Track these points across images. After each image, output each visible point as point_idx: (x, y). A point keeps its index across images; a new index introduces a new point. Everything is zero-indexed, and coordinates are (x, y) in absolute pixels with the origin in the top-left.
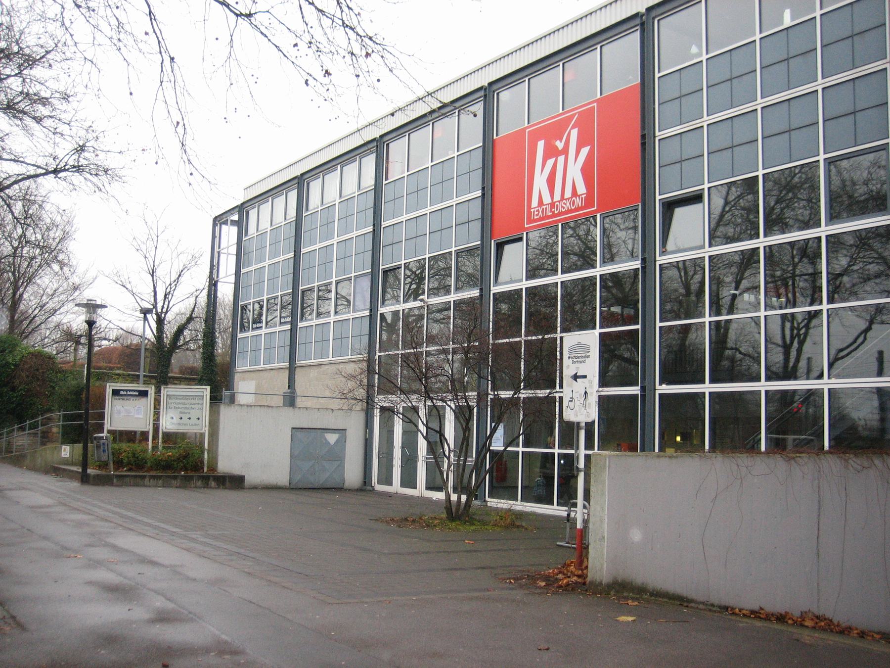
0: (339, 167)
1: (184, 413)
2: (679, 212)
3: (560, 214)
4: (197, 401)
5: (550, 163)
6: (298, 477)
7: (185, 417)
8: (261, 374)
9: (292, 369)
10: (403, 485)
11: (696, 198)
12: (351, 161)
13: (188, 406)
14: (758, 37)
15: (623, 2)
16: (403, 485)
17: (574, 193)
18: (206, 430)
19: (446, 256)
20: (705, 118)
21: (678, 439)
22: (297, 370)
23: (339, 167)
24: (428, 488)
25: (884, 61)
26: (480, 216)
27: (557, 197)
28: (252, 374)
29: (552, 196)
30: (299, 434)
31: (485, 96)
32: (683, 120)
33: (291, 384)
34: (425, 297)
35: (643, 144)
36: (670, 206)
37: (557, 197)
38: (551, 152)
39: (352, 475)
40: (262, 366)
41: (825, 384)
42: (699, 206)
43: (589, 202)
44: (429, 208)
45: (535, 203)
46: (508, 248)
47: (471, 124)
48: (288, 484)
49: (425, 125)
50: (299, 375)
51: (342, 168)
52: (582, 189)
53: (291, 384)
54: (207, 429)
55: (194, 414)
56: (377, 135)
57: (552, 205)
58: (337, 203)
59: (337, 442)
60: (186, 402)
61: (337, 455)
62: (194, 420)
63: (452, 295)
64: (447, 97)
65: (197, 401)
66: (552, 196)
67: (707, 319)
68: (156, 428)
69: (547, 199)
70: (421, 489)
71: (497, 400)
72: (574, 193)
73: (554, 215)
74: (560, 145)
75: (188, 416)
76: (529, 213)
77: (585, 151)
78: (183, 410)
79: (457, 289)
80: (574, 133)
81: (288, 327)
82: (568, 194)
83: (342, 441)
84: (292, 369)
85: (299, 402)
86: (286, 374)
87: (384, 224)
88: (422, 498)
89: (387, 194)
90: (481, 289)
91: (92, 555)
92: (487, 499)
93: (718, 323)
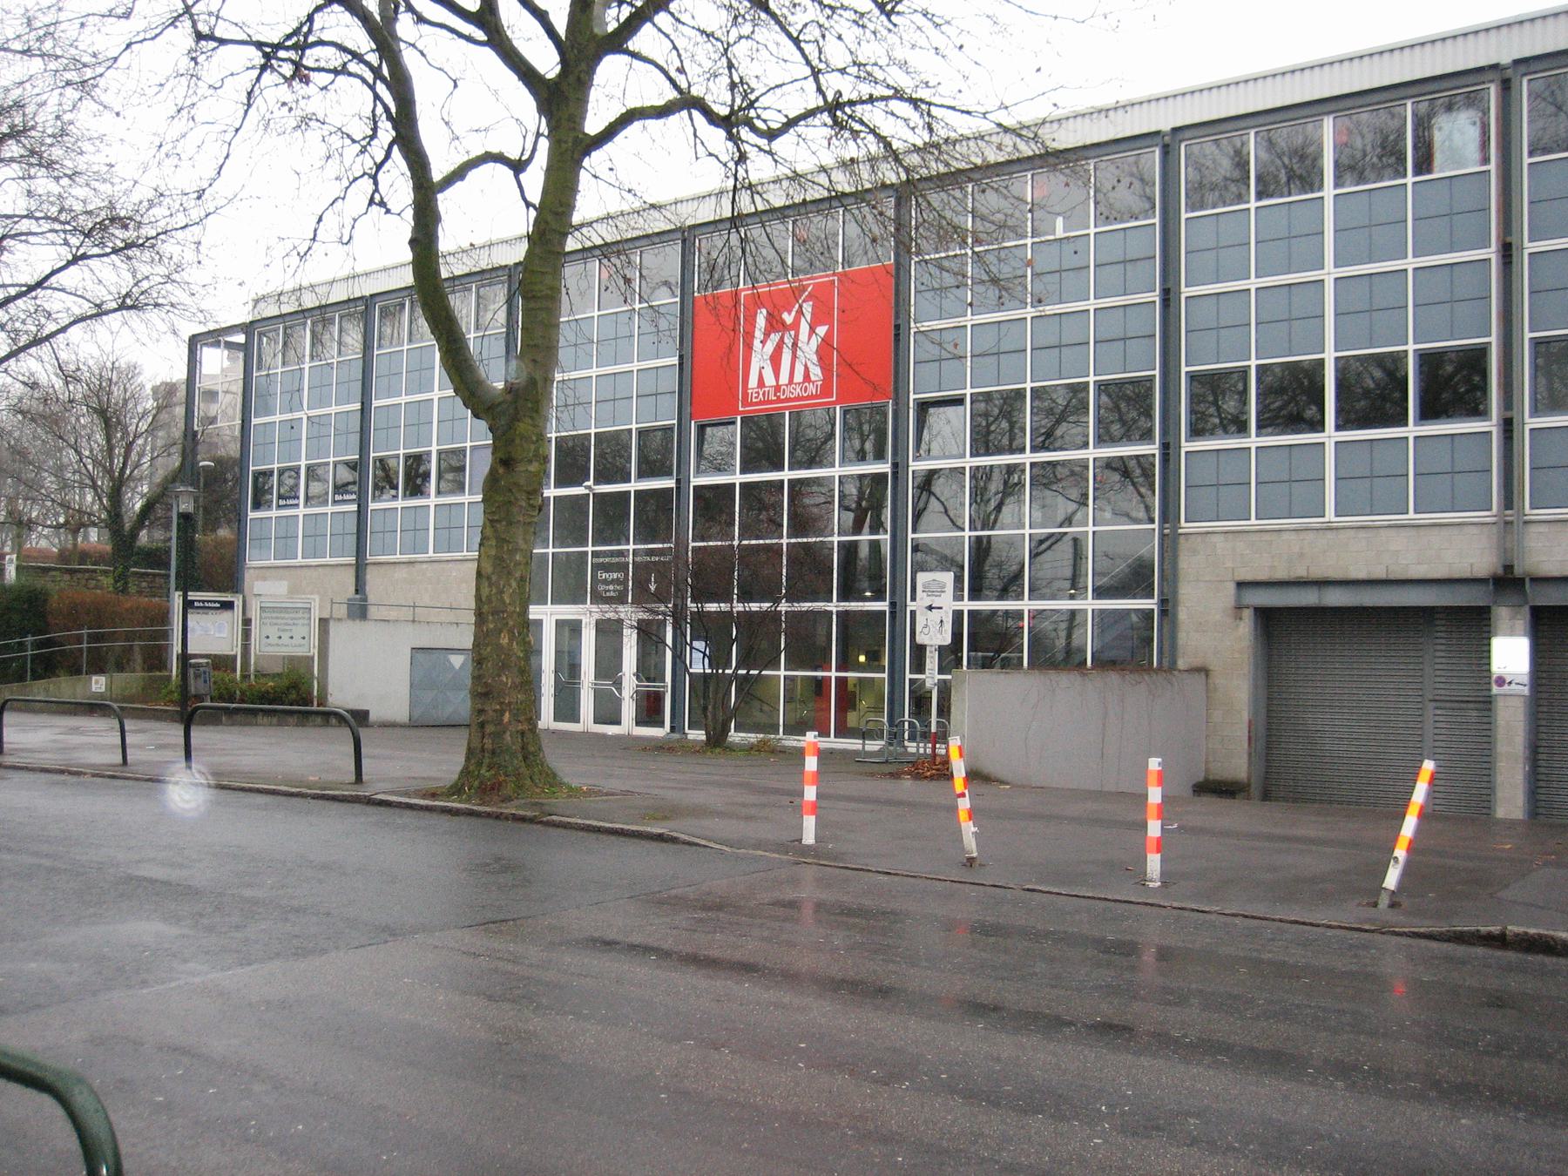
3: (788, 400)
5: (775, 337)
6: (416, 715)
7: (285, 636)
8: (299, 571)
9: (360, 568)
10: (598, 720)
11: (959, 401)
14: (596, 313)
17: (807, 377)
18: (315, 652)
21: (862, 658)
22: (369, 569)
27: (784, 379)
28: (286, 572)
29: (777, 379)
30: (420, 656)
32: (1064, 298)
33: (360, 587)
34: (590, 483)
35: (897, 335)
37: (784, 379)
38: (775, 324)
40: (300, 560)
41: (1026, 605)
42: (960, 408)
43: (826, 390)
45: (753, 382)
46: (936, 416)
50: (371, 576)
52: (816, 373)
53: (360, 587)
55: (299, 631)
56: (1166, 126)
57: (777, 388)
64: (1064, 139)
66: (777, 379)
67: (785, 541)
69: (770, 380)
70: (628, 724)
71: (700, 616)
72: (807, 377)
73: (779, 400)
74: (788, 318)
76: (745, 394)
77: (822, 330)
80: (808, 308)
81: (354, 507)
82: (799, 377)
84: (360, 568)
85: (373, 612)
86: (351, 573)
88: (629, 737)
91: (160, 890)
93: (979, 538)
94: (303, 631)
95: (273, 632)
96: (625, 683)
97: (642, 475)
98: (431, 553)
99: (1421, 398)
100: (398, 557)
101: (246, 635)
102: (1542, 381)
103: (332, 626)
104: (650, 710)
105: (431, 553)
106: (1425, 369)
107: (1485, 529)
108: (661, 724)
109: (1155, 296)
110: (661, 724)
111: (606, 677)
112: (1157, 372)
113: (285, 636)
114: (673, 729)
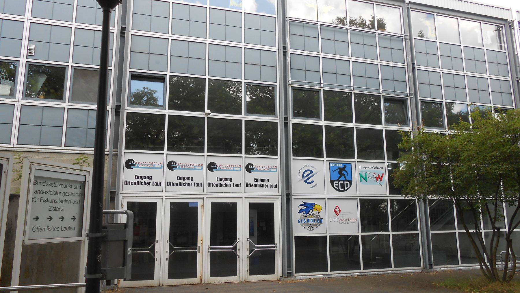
13: (61, 197)
78: (54, 205)
104: (262, 263)
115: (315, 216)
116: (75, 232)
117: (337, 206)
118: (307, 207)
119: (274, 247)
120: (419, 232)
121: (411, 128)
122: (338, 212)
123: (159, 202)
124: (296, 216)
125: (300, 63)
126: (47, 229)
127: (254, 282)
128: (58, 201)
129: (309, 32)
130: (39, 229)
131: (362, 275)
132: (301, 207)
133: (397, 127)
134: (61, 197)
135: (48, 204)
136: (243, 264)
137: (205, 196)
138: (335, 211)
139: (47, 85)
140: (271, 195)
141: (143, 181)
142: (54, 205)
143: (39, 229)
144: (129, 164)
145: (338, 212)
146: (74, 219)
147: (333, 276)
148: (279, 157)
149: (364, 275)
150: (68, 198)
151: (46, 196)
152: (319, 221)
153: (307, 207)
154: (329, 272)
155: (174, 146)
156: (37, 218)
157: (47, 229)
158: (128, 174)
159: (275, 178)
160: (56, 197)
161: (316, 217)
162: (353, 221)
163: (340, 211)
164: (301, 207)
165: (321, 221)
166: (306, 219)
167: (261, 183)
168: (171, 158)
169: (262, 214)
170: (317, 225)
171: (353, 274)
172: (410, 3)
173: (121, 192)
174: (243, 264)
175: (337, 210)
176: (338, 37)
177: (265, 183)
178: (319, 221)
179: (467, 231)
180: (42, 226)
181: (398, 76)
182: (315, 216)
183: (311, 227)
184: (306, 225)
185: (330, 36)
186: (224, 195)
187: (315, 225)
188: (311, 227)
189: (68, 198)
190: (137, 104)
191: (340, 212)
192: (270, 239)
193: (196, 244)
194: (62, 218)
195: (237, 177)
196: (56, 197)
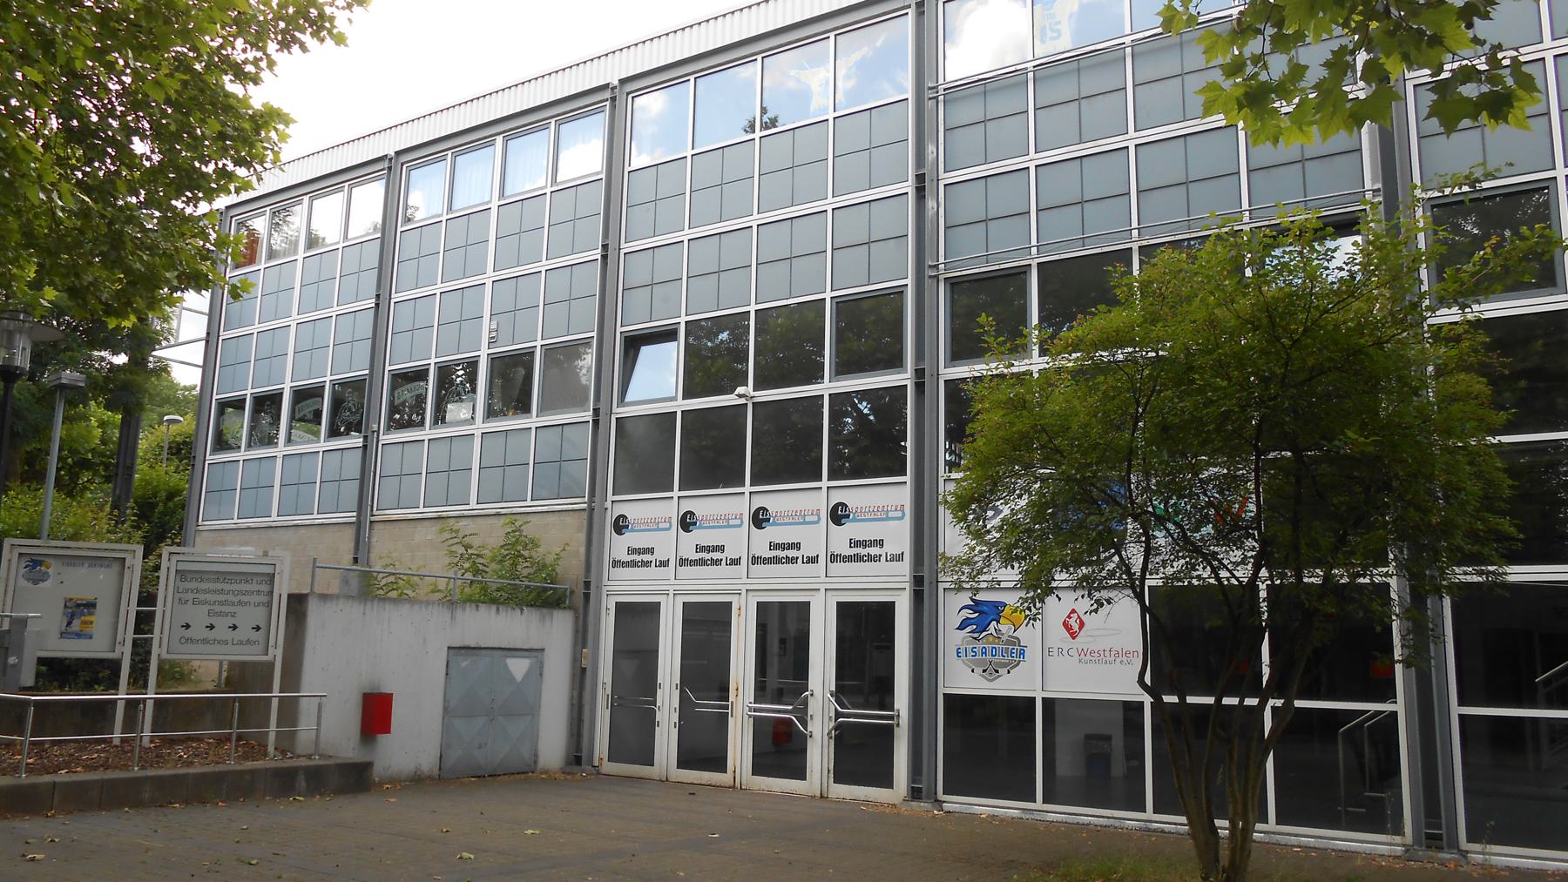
0: (499, 139)
1: (220, 614)
2: (646, 351)
4: (254, 587)
7: (222, 624)
11: (668, 335)
12: (335, 189)
13: (231, 598)
15: (780, 2)
16: (761, 766)
18: (277, 654)
19: (736, 323)
20: (756, 216)
23: (499, 139)
24: (683, 763)
25: (1540, 47)
26: (370, 335)
31: (390, 168)
36: (634, 343)
39: (552, 746)
44: (687, 231)
47: (369, 199)
48: (436, 772)
49: (747, 60)
51: (455, 157)
54: (279, 653)
58: (494, 206)
59: (527, 675)
60: (227, 587)
61: (524, 706)
62: (245, 632)
63: (534, 418)
65: (254, 587)
68: (141, 651)
75: (231, 621)
78: (218, 608)
79: (249, 446)
83: (538, 671)
86: (350, 533)
87: (396, 297)
89: (407, 246)
90: (365, 438)
92: (941, 796)
94: (258, 616)
95: (198, 617)
96: (815, 707)
97: (845, 367)
98: (274, 517)
99: (838, 351)
100: (422, 511)
101: (144, 622)
102: (498, 381)
103: (314, 611)
104: (862, 755)
105: (274, 517)
106: (866, 305)
107: (568, 519)
108: (886, 781)
109: (909, 187)
110: (886, 781)
111: (779, 697)
112: (909, 281)
113: (222, 624)
114: (915, 794)
115: (1004, 638)
116: (259, 648)
117: (1073, 611)
118: (981, 612)
119: (891, 718)
120: (1399, 707)
121: (928, 367)
122: (1076, 628)
123: (734, 600)
124: (952, 637)
125: (970, 206)
126: (205, 641)
127: (841, 802)
128: (225, 603)
129: (998, 105)
130: (190, 640)
131: (1149, 830)
132: (967, 613)
133: (966, 368)
134: (231, 598)
135: (207, 607)
136: (819, 755)
137: (744, 588)
138: (1065, 624)
139: (20, 467)
140: (887, 580)
141: (641, 558)
142: (218, 608)
143: (190, 640)
144: (620, 526)
145: (1076, 628)
146: (258, 628)
147: (1051, 817)
148: (908, 478)
149: (1155, 831)
150: (245, 599)
151: (202, 597)
152: (1016, 652)
153: (981, 612)
154: (1039, 804)
155: (692, 480)
156: (188, 626)
157: (205, 641)
158: (618, 546)
159: (899, 537)
160: (222, 598)
161: (1008, 642)
162: (1121, 655)
163: (1082, 625)
164: (967, 613)
165: (1022, 653)
166: (979, 646)
167: (862, 552)
168: (837, 497)
169: (865, 627)
170: (1011, 666)
171: (1117, 823)
172: (623, 82)
173: (605, 581)
174: (819, 755)
175: (1072, 622)
176: (1092, 83)
177: (791, 553)
178: (1016, 652)
179: (1182, 699)
180: (196, 637)
181: (1204, 160)
182: (1004, 638)
183: (991, 671)
184: (979, 663)
185: (1067, 89)
186: (782, 583)
187: (1005, 665)
188: (991, 671)
189: (245, 599)
190: (1538, 286)
191: (1081, 628)
192: (882, 692)
193: (1020, 708)
194: (235, 627)
195: (737, 541)
196: (222, 598)
